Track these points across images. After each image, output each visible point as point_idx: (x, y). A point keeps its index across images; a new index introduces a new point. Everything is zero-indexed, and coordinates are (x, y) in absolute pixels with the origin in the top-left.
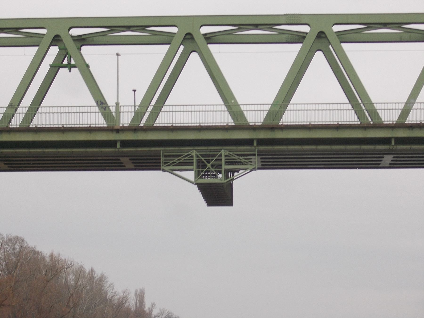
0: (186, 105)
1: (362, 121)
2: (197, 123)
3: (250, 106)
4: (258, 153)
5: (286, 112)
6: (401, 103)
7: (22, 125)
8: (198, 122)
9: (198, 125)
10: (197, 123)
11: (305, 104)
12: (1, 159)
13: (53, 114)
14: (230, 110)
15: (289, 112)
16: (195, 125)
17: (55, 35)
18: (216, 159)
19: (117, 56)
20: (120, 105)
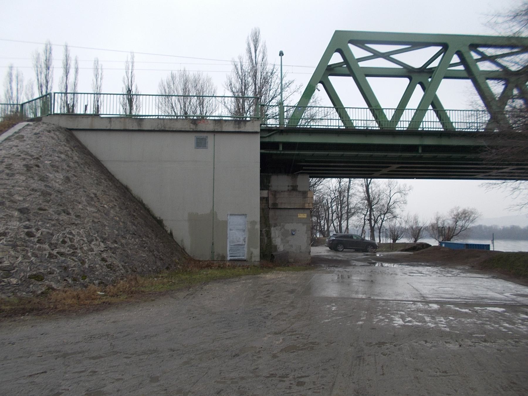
0: (107, 94)
1: (348, 126)
2: (336, 126)
3: (362, 109)
4: (263, 151)
5: (410, 120)
6: (392, 109)
7: (290, 124)
8: (337, 125)
9: (337, 127)
10: (336, 126)
11: (361, 108)
12: (527, 178)
13: (432, 123)
14: (442, 122)
15: (407, 120)
16: (335, 127)
17: (350, 39)
18: (17, 136)
19: (280, 57)
20: (284, 105)
